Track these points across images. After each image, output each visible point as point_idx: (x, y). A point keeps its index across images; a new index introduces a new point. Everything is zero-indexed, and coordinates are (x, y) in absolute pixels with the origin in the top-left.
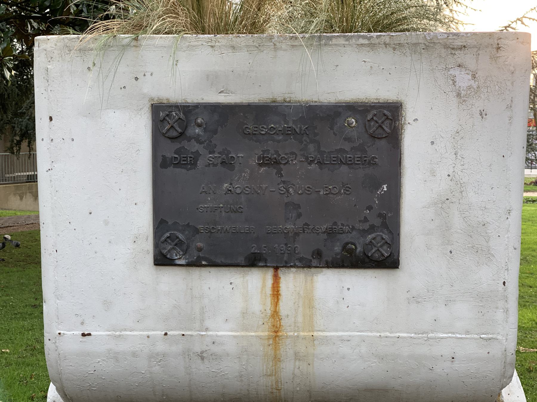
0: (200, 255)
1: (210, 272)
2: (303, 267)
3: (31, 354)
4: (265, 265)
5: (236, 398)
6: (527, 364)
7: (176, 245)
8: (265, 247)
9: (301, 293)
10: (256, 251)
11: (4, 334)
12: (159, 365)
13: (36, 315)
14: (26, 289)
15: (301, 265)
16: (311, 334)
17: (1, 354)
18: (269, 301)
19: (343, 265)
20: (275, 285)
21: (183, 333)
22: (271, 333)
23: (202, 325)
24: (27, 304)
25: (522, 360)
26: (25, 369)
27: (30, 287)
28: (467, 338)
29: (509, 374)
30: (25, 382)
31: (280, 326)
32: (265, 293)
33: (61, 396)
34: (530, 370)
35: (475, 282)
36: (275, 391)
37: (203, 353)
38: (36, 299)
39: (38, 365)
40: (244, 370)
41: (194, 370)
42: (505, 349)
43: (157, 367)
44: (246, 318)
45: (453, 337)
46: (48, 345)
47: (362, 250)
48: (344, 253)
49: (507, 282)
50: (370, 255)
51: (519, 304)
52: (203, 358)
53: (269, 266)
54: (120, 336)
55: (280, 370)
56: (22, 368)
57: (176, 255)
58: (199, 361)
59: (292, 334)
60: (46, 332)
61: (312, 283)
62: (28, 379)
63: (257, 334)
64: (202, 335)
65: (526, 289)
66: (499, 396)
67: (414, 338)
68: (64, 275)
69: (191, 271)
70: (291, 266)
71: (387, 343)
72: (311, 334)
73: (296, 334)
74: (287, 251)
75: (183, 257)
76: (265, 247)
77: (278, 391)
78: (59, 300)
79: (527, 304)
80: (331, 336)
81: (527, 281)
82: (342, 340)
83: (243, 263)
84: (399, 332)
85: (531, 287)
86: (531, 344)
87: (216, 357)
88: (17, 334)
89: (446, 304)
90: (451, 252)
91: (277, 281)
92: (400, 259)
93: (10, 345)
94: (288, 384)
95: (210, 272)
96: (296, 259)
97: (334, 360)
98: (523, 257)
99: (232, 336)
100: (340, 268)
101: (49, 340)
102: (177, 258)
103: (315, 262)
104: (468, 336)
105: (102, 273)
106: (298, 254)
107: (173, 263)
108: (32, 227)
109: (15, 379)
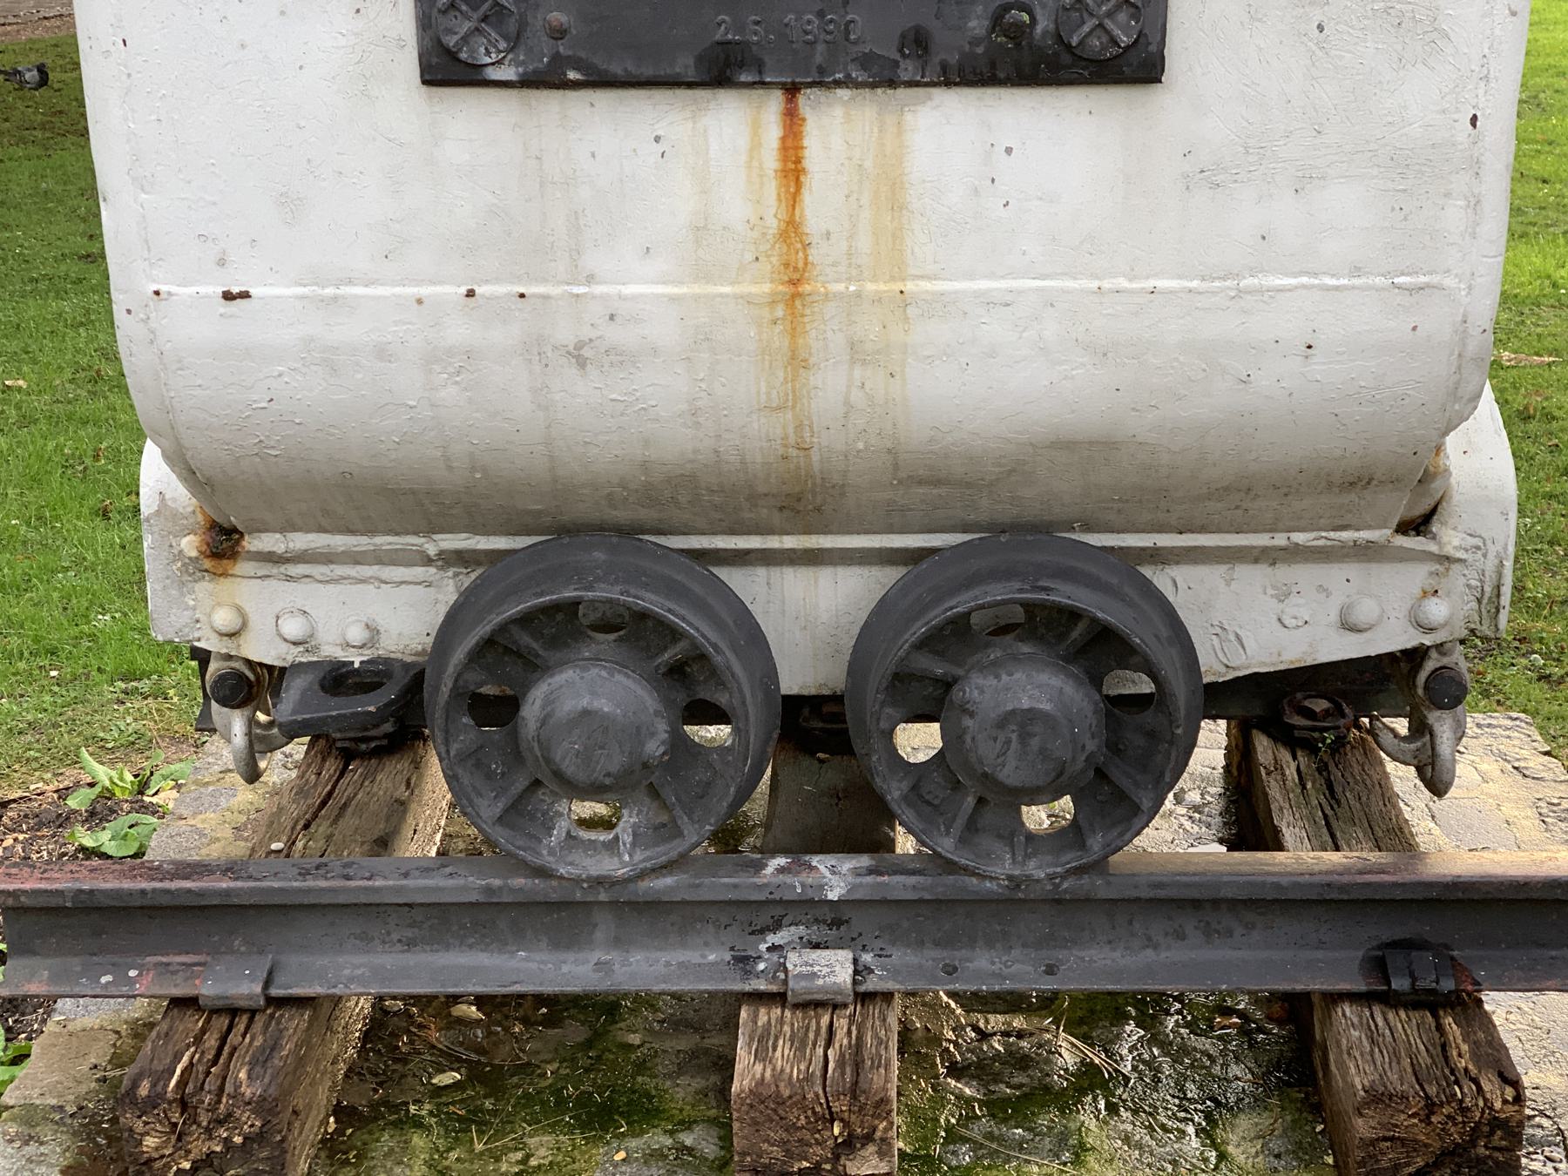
0: (561, 49)
1: (592, 105)
2: (873, 86)
3: (89, 392)
4: (757, 79)
5: (682, 475)
6: (1520, 398)
7: (485, 19)
8: (757, 23)
9: (868, 164)
10: (730, 37)
11: (6, 337)
12: (456, 383)
13: (94, 281)
14: (60, 209)
15: (865, 78)
16: (899, 286)
17: (3, 392)
18: (771, 189)
19: (994, 75)
20: (789, 143)
21: (522, 290)
22: (781, 288)
23: (576, 266)
24: (67, 251)
25: (1506, 389)
26: (76, 432)
27: (70, 203)
28: (1354, 287)
29: (1471, 388)
30: (81, 468)
31: (806, 264)
32: (761, 168)
33: (179, 476)
34: (1525, 415)
35: (1390, 119)
36: (793, 452)
37: (581, 348)
38: (91, 236)
39: (111, 422)
40: (703, 394)
41: (557, 397)
42: (1464, 316)
43: (452, 390)
44: (705, 243)
45: (1313, 286)
46: (127, 329)
47: (1052, 26)
48: (996, 37)
49: (1483, 115)
50: (1075, 41)
51: (1512, 234)
52: (582, 363)
53: (769, 83)
54: (335, 298)
55: (808, 393)
56: (67, 431)
57: (488, 53)
58: (573, 371)
59: (840, 287)
60: (116, 290)
61: (900, 133)
62: (88, 461)
63: (738, 289)
64: (578, 295)
65: (1530, 188)
66: (1437, 454)
67: (1200, 293)
68: (154, 117)
69: (534, 103)
70: (838, 84)
71: (1119, 308)
72: (899, 286)
73: (852, 288)
74: (823, 36)
75: (510, 56)
76: (757, 23)
77: (802, 453)
78: (146, 193)
79: (1532, 230)
80: (956, 292)
81: (1536, 166)
82: (989, 302)
83: (691, 75)
84: (1156, 275)
85: (1544, 181)
86: (1535, 343)
87: (621, 358)
88: (45, 337)
89: (1298, 187)
90: (1321, 28)
91: (795, 128)
92: (1166, 51)
93: (25, 369)
94: (832, 431)
95: (592, 105)
96: (853, 60)
97: (964, 360)
98: (1527, 93)
99: (663, 295)
100: (983, 85)
101: (129, 312)
102: (489, 60)
103: (907, 70)
104: (1356, 282)
105: (268, 109)
106: (855, 43)
107: (480, 78)
108: (58, 27)
109: (50, 459)
